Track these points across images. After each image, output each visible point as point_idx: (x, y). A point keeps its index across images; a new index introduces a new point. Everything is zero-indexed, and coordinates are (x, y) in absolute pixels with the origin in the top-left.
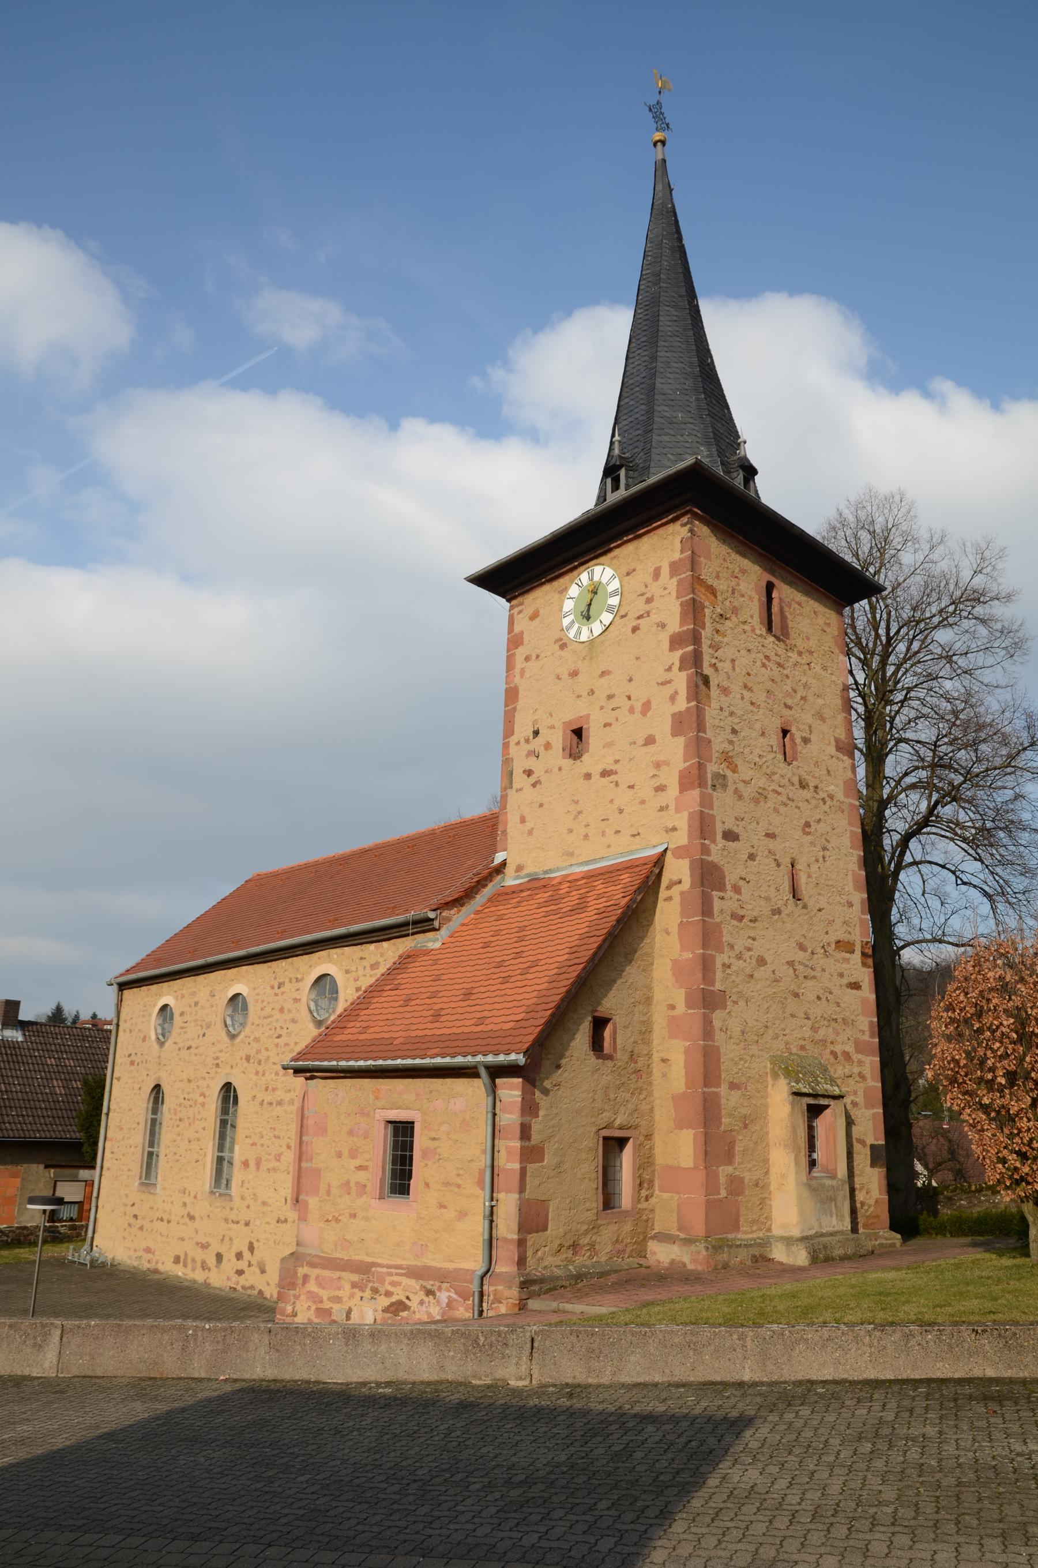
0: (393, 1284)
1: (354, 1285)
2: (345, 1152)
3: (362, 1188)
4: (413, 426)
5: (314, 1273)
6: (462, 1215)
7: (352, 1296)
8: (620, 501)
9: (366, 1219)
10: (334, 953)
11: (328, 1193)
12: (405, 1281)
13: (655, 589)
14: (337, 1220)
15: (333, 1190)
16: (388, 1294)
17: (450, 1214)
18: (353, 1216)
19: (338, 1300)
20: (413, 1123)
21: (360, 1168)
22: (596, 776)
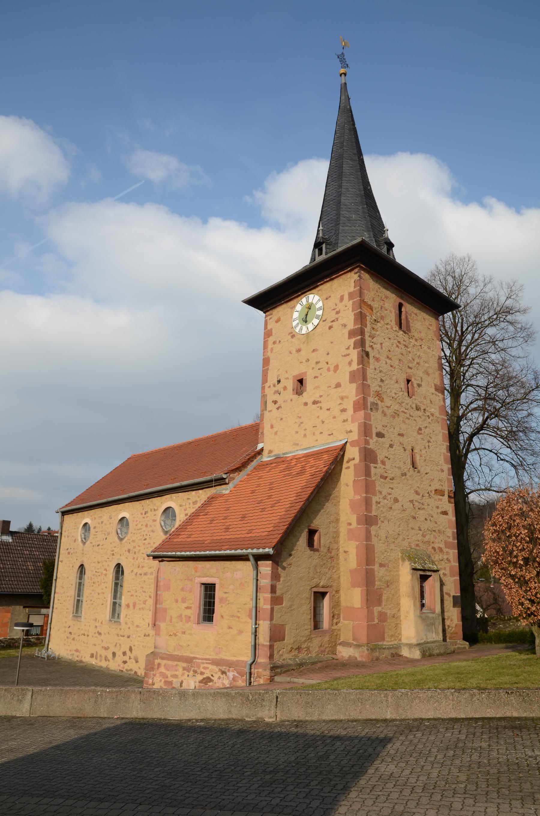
0: (205, 668)
1: (184, 669)
2: (180, 600)
3: (188, 618)
4: (215, 222)
5: (163, 662)
6: (240, 632)
7: (183, 674)
8: (323, 261)
9: (190, 634)
10: (174, 496)
11: (171, 621)
12: (211, 667)
13: (341, 306)
14: (175, 635)
15: (173, 619)
16: (202, 673)
17: (234, 632)
18: (184, 633)
19: (176, 676)
20: (215, 584)
21: (187, 608)
22: (310, 404)
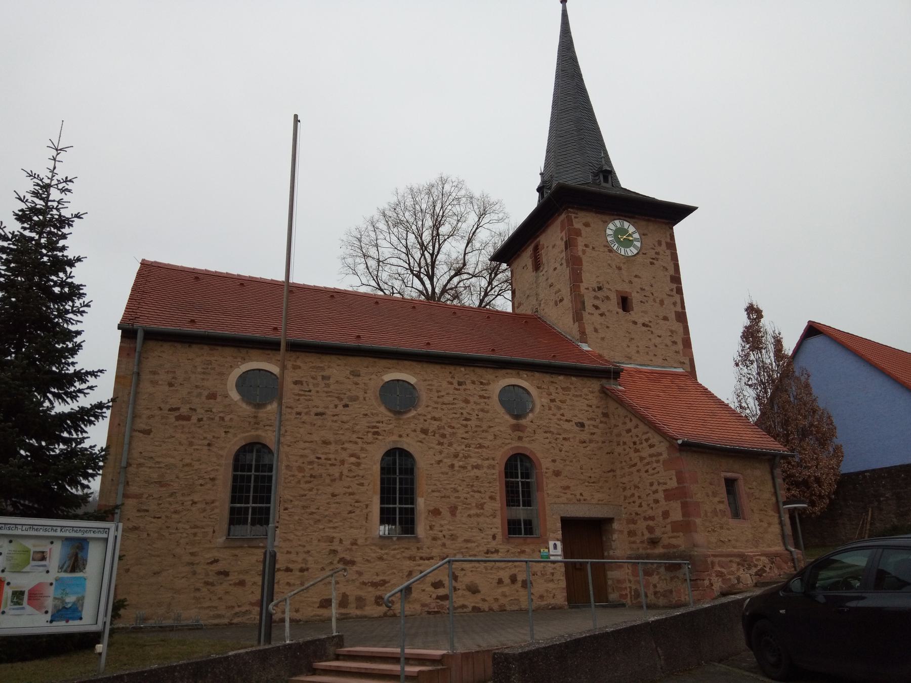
0: (757, 560)
1: (738, 564)
2: (710, 493)
3: (723, 513)
4: (194, 346)
5: (716, 560)
6: (770, 524)
7: (738, 570)
8: (547, 227)
9: (728, 529)
10: (417, 367)
11: (706, 515)
12: (762, 558)
13: (658, 249)
14: (714, 531)
15: (709, 514)
16: (756, 566)
17: (765, 525)
18: (722, 528)
19: (732, 573)
20: (398, 413)
21: (719, 502)
22: (639, 325)
